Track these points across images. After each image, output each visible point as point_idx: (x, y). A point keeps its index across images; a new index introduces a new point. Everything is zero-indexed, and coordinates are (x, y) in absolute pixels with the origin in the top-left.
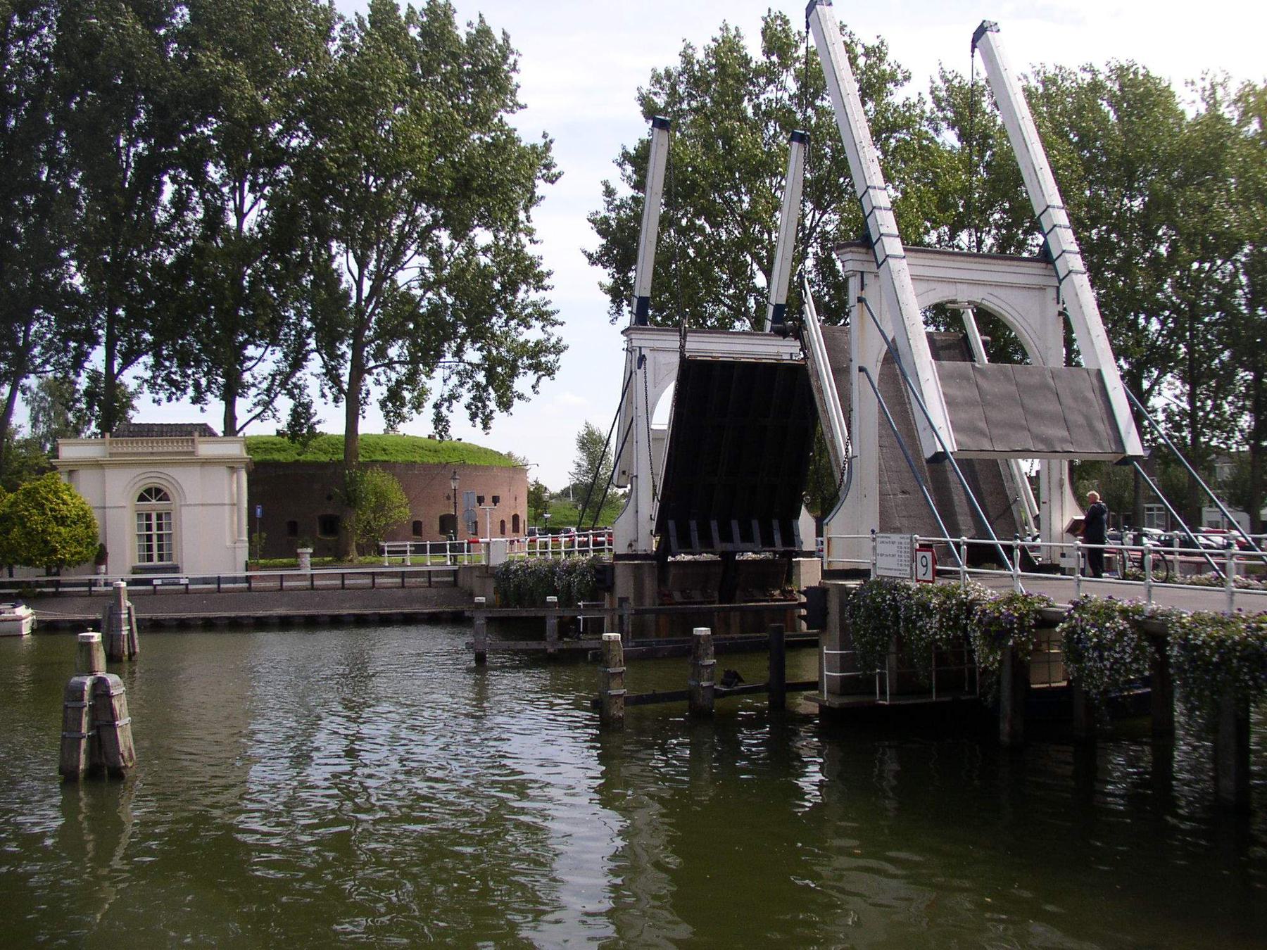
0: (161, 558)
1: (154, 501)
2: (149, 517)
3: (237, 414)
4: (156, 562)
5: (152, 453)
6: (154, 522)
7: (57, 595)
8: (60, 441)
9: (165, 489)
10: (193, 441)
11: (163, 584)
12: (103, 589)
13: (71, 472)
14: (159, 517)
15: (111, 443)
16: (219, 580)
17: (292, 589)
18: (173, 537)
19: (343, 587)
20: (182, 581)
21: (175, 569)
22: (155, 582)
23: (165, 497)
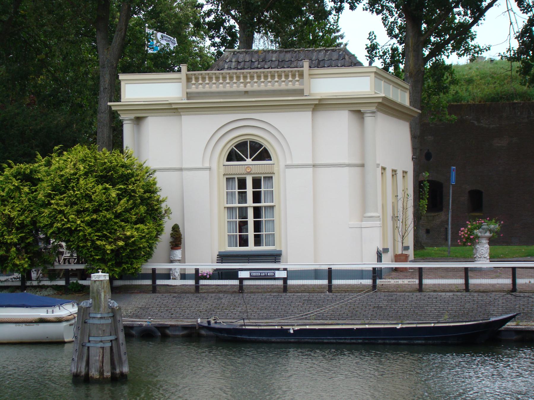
0: (258, 241)
1: (249, 161)
2: (242, 183)
3: (353, 53)
4: (251, 247)
5: (246, 93)
6: (250, 190)
7: (154, 289)
8: (122, 77)
9: (266, 145)
10: (301, 75)
11: (252, 278)
12: (179, 282)
13: (138, 120)
14: (257, 183)
15: (189, 79)
16: (330, 274)
17: (436, 289)
18: (276, 209)
19: (330, 287)
20: (278, 274)
21: (275, 257)
22: (242, 275)
23: (265, 155)
